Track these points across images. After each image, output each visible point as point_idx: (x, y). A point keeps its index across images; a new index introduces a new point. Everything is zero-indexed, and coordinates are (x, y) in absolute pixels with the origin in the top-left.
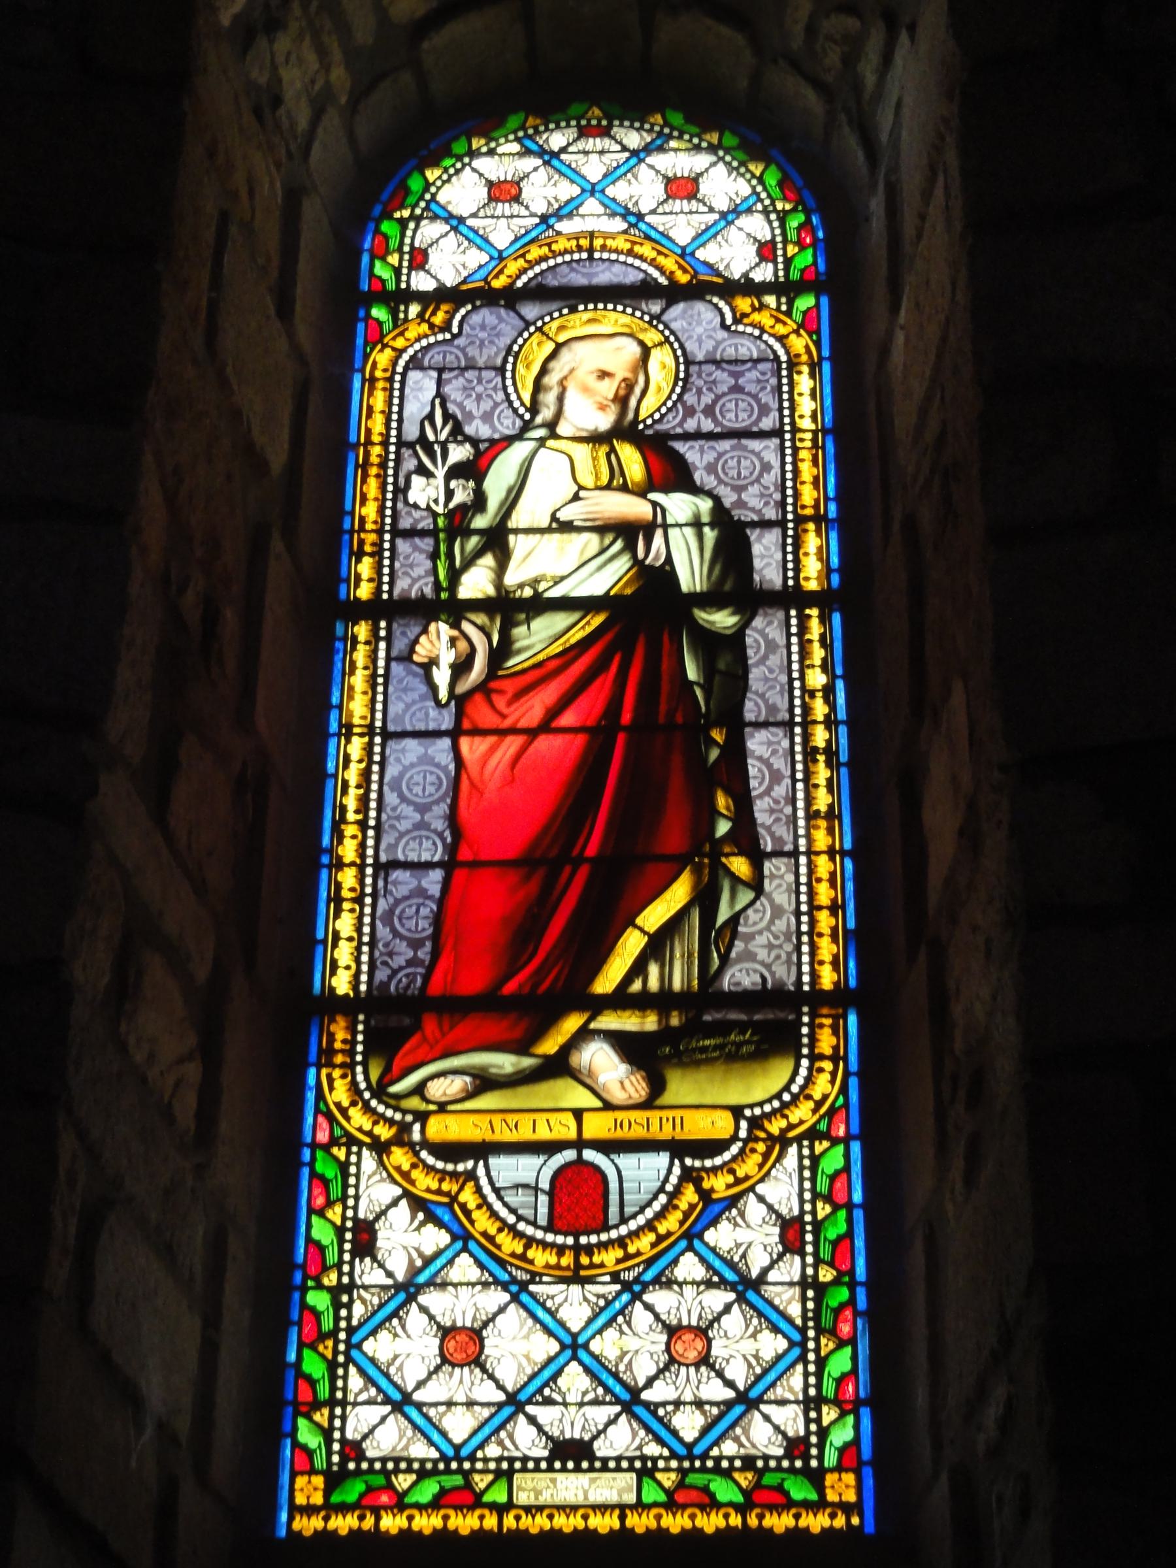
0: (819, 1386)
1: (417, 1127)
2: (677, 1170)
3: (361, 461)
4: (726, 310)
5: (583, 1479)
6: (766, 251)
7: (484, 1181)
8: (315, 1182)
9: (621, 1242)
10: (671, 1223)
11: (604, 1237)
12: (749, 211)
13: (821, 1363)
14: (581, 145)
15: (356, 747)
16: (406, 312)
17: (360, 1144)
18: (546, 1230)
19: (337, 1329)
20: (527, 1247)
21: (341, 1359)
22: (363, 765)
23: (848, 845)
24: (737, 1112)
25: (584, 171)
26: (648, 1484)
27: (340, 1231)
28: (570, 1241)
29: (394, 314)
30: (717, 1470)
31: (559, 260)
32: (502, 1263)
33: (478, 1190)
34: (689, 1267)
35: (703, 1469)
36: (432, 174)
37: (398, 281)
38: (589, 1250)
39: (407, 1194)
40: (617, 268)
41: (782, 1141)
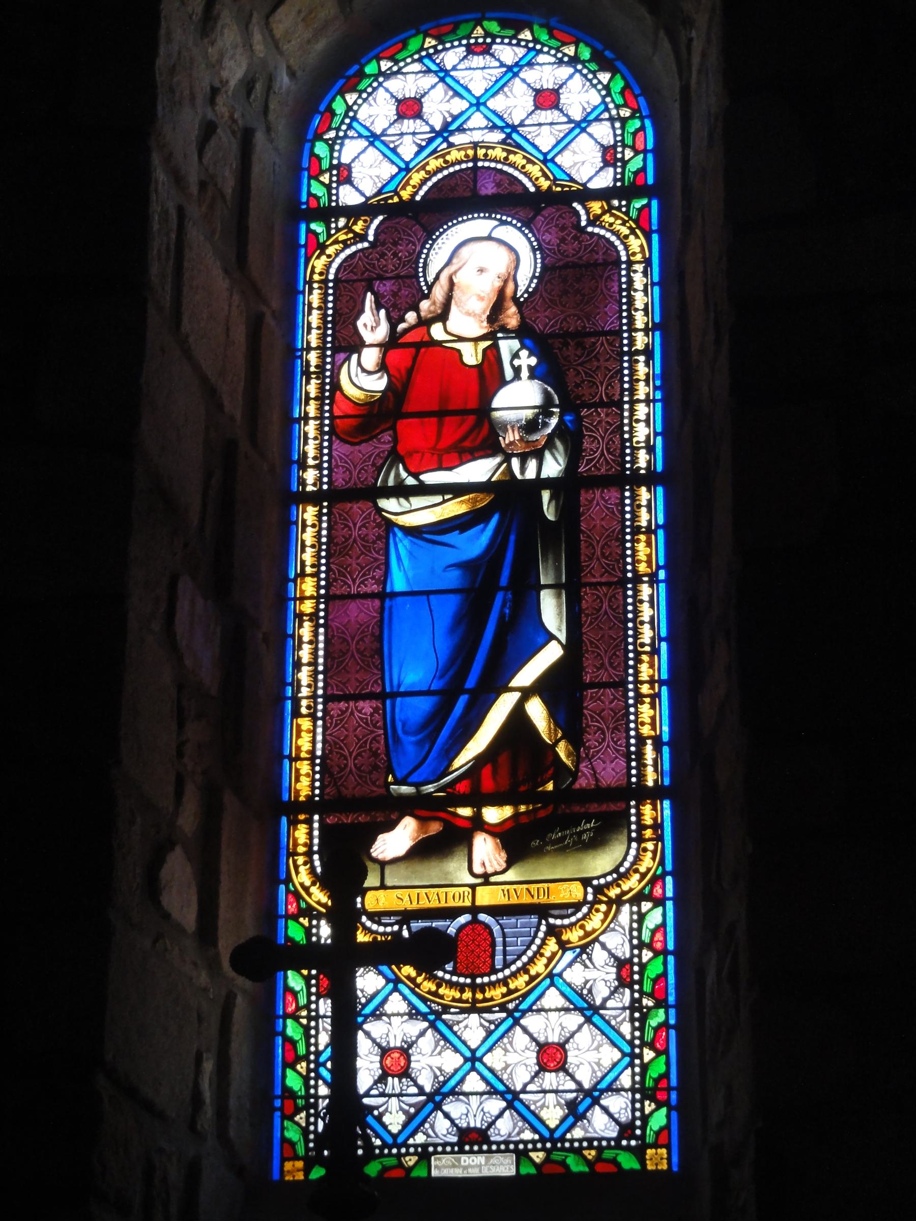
2: (543, 928)
3: (308, 279)
5: (480, 1159)
6: (609, 156)
8: (287, 1044)
9: (505, 982)
11: (493, 978)
12: (597, 119)
14: (466, 64)
19: (309, 1053)
23: (664, 676)
24: (586, 882)
27: (305, 1132)
30: (572, 1150)
34: (553, 998)
35: (563, 1149)
36: (351, 98)
38: (482, 988)
41: (619, 901)
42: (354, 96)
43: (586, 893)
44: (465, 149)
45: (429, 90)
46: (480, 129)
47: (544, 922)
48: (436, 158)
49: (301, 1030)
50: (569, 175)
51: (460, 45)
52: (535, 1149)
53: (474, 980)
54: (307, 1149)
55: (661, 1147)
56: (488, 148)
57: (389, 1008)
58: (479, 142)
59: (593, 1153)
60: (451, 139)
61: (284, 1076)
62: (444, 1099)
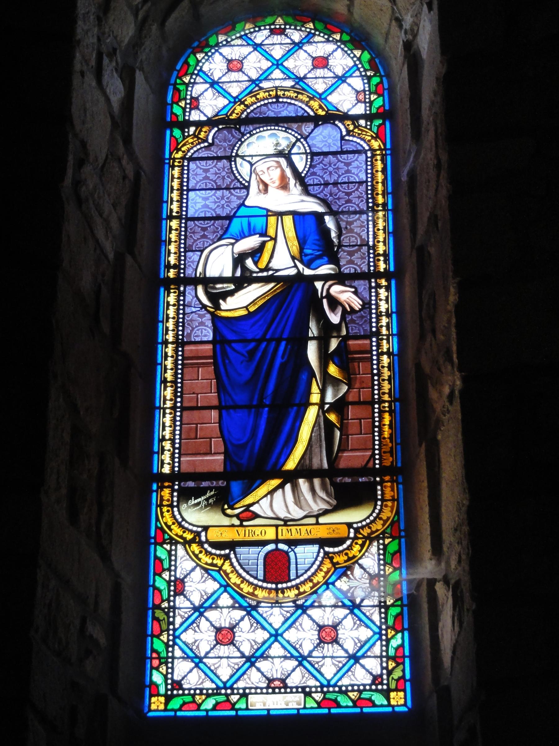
0: (387, 651)
1: (203, 534)
2: (321, 555)
4: (342, 127)
7: (234, 560)
9: (297, 587)
10: (319, 578)
11: (289, 584)
13: (388, 641)
15: (170, 350)
16: (188, 132)
17: (177, 542)
18: (264, 581)
19: (170, 565)
20: (255, 589)
21: (171, 643)
22: (175, 332)
24: (349, 525)
25: (273, 53)
26: (308, 699)
27: (169, 582)
28: (274, 586)
29: (183, 132)
30: (340, 692)
31: (262, 103)
32: (243, 597)
33: (232, 564)
36: (200, 56)
37: (184, 115)
39: (198, 565)
40: (291, 108)
42: (202, 55)
43: (349, 532)
44: (268, 91)
45: (247, 55)
46: (279, 79)
47: (322, 550)
48: (251, 97)
49: (166, 553)
50: (336, 108)
51: (265, 29)
52: (316, 692)
53: (277, 585)
54: (167, 690)
55: (400, 691)
56: (285, 91)
57: (221, 603)
58: (279, 87)
59: (355, 693)
60: (261, 85)
61: (151, 675)
62: (257, 660)
